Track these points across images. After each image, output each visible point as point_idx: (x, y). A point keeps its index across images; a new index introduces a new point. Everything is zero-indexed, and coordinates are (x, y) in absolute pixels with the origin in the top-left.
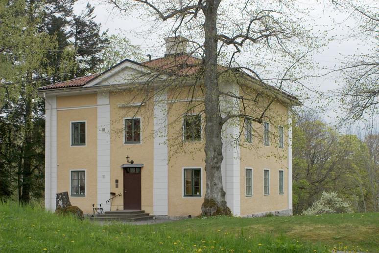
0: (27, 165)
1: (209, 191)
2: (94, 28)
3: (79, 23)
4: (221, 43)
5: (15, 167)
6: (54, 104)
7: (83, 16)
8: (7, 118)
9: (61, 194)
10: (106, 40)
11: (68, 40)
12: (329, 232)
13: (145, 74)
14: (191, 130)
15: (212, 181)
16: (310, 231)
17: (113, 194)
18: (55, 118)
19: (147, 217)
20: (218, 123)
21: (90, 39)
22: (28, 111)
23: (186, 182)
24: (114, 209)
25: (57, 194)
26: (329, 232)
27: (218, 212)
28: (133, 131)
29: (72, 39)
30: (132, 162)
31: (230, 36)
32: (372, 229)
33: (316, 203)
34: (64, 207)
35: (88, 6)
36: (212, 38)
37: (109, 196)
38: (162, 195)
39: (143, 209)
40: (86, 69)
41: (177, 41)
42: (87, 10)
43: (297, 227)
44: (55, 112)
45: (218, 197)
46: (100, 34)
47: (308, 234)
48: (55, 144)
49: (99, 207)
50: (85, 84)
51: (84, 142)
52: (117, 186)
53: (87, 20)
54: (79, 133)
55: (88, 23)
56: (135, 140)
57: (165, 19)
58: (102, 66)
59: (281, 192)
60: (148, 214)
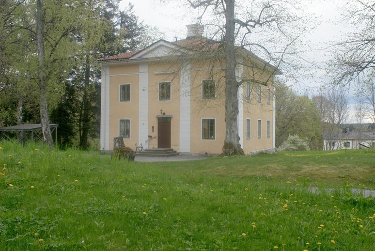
0: (86, 115)
1: (228, 137)
2: (134, 19)
3: (123, 16)
4: (239, 25)
5: (77, 116)
6: (108, 72)
7: (126, 11)
8: (73, 82)
9: (117, 138)
10: (142, 28)
11: (115, 27)
12: (333, 171)
13: (176, 51)
14: (209, 89)
15: (230, 129)
16: (317, 170)
17: (150, 137)
18: (108, 81)
19: (175, 154)
20: (232, 86)
21: (131, 28)
22: (87, 77)
23: (204, 129)
24: (151, 148)
25: (115, 138)
26: (333, 171)
27: (235, 152)
28: (165, 92)
29: (118, 27)
30: (164, 114)
31: (245, 21)
32: (367, 169)
33: (285, 143)
34: (119, 148)
35: (130, 4)
36: (231, 22)
37: (147, 138)
38: (186, 138)
39: (172, 147)
40: (128, 48)
41: (197, 28)
42: (129, 7)
43: (305, 166)
44: (108, 77)
45: (234, 141)
46: (138, 24)
47: (316, 173)
48: (108, 100)
49: (140, 146)
50: (130, 57)
51: (130, 99)
52: (153, 131)
53: (129, 14)
54: (126, 93)
55: (130, 16)
56: (167, 98)
57: (195, 7)
58: (138, 46)
59: (268, 136)
60: (176, 152)
